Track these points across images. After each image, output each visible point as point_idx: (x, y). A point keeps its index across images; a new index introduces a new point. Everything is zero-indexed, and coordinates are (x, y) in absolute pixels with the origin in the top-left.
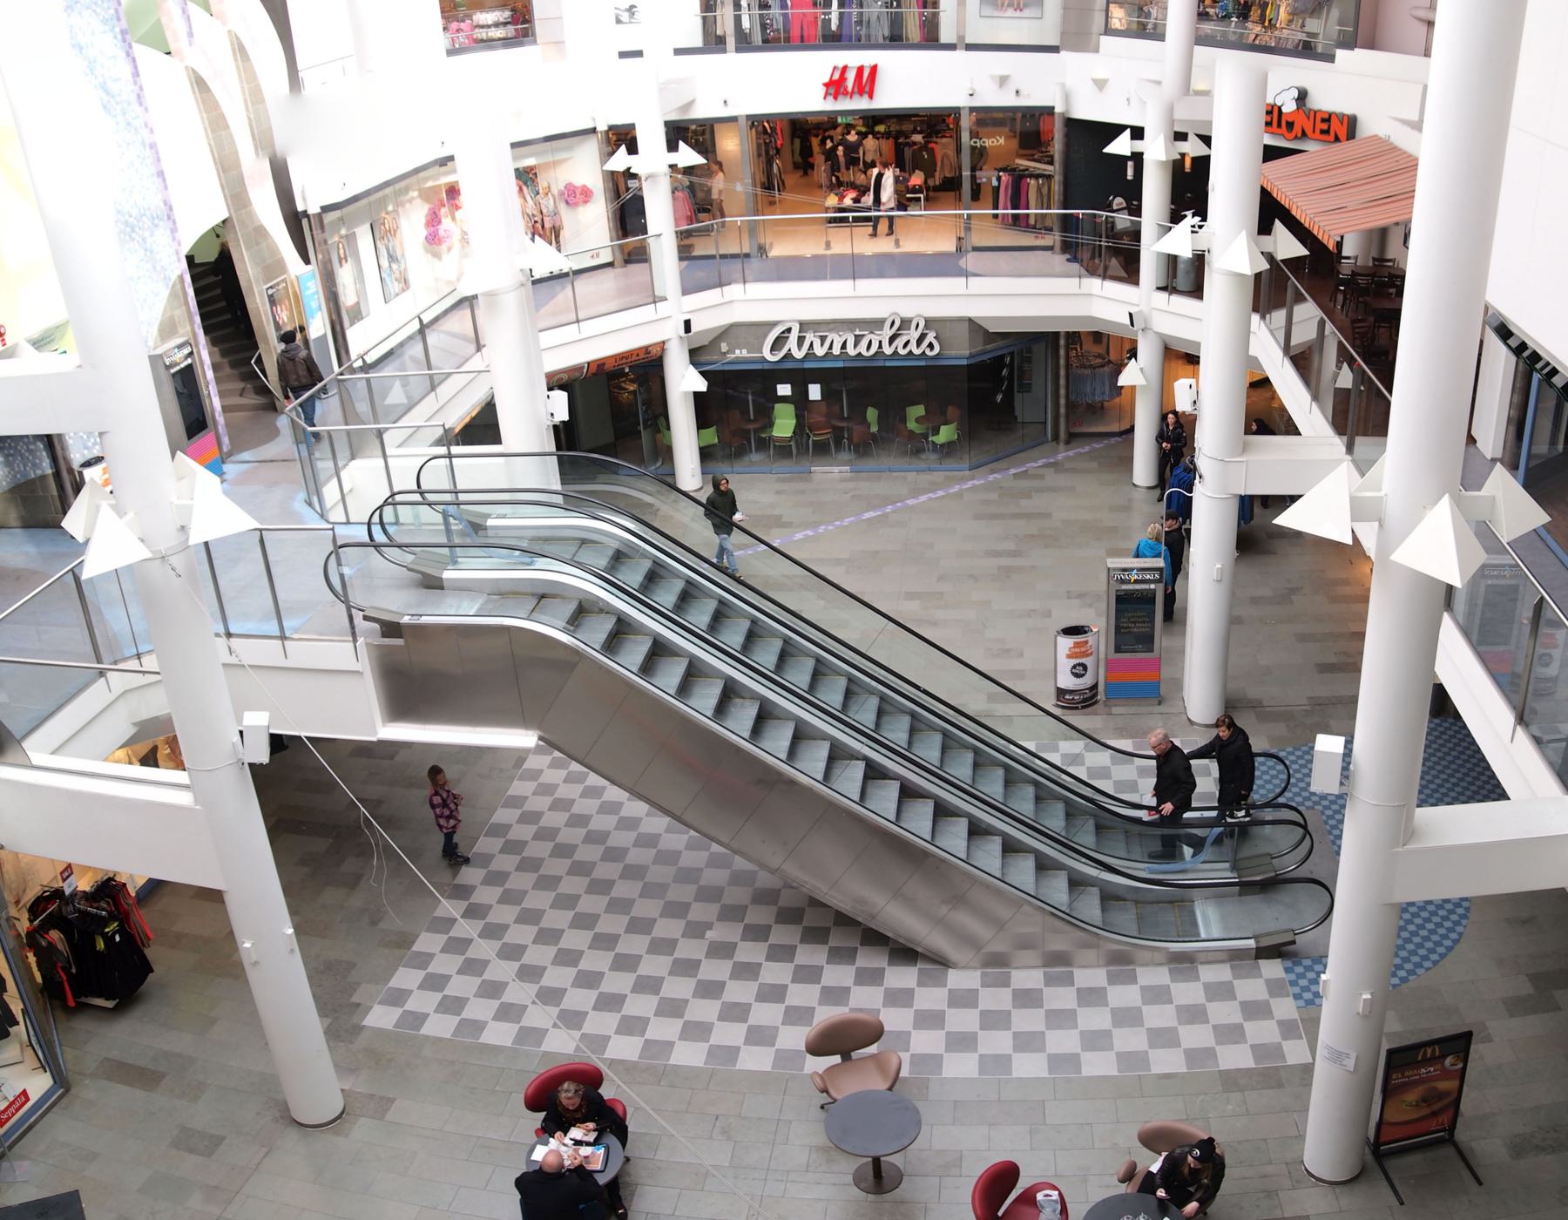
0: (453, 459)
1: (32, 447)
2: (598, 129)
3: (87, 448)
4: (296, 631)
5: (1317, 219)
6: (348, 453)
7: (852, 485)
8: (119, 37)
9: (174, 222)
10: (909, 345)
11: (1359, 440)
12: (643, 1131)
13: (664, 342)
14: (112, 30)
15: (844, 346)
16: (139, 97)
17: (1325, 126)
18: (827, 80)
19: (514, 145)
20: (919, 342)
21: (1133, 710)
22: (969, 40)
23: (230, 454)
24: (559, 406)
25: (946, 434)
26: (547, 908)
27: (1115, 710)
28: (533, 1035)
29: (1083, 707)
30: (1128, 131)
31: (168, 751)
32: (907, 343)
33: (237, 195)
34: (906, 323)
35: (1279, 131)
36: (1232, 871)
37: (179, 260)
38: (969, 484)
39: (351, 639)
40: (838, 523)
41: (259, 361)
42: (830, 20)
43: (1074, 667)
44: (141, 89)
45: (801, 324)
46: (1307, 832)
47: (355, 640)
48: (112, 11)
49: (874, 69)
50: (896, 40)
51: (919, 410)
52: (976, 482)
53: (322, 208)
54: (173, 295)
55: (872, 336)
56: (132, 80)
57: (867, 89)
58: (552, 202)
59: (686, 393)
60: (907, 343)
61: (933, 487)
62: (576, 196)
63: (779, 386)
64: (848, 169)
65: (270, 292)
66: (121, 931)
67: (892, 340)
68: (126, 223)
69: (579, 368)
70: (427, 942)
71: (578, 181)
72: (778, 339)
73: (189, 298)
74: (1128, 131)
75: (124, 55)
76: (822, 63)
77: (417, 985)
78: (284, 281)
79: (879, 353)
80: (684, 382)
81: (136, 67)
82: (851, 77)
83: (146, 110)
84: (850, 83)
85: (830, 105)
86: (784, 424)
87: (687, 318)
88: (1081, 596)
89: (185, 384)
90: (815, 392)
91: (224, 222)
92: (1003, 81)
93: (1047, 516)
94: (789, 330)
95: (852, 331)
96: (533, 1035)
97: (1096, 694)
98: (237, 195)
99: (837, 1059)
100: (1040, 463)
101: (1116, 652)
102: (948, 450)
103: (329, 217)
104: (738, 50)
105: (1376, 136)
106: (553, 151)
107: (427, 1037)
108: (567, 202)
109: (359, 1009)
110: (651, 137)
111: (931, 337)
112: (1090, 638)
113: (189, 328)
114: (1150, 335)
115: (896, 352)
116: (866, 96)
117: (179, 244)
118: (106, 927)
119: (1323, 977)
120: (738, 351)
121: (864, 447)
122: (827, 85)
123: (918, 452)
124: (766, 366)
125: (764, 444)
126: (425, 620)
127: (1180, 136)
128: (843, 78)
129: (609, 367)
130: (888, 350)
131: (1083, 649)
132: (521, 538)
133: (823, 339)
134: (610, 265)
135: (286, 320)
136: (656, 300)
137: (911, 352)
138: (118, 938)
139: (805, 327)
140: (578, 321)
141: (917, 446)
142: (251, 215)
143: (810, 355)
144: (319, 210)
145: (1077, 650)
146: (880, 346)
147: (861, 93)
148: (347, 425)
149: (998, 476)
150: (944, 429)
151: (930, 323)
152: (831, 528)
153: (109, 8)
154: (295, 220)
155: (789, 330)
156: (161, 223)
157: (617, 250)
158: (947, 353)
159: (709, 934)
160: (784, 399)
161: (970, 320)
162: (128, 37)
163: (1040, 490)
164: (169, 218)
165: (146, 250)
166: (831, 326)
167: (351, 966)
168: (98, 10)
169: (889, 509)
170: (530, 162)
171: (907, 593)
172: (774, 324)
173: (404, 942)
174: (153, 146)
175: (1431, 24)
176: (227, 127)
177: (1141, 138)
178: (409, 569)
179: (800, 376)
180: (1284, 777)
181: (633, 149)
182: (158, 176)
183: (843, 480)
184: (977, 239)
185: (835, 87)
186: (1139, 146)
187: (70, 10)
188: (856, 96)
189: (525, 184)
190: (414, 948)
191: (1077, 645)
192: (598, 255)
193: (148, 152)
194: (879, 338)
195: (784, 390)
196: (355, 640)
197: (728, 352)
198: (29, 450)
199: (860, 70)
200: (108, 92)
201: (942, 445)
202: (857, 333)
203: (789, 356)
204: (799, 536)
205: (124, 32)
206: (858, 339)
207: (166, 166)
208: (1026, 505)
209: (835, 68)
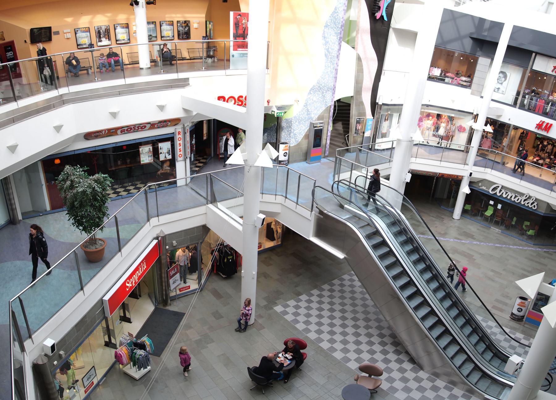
1: (274, 134)
2: (474, 114)
3: (285, 139)
4: (302, 203)
7: (498, 235)
8: (339, 38)
9: (335, 91)
10: (529, 204)
12: (311, 366)
13: (463, 176)
14: (337, 36)
15: (511, 197)
16: (338, 56)
18: (538, 123)
19: (423, 105)
20: (532, 204)
21: (531, 328)
23: (327, 156)
24: (408, 178)
25: (531, 232)
26: (337, 303)
27: (526, 325)
28: (308, 331)
29: (517, 321)
31: (274, 223)
32: (528, 203)
33: (358, 90)
34: (530, 197)
37: (332, 101)
38: (531, 248)
39: (311, 210)
41: (348, 136)
42: (547, 109)
43: (519, 308)
44: (339, 54)
45: (502, 186)
47: (312, 211)
48: (339, 31)
49: (551, 125)
51: (527, 223)
52: (533, 249)
53: (383, 104)
54: (326, 109)
55: (520, 197)
56: (337, 51)
58: (454, 128)
59: (464, 193)
60: (528, 203)
61: (521, 245)
62: (461, 129)
63: (491, 201)
64: (541, 151)
65: (358, 120)
66: (232, 259)
67: (525, 200)
68: (319, 87)
69: (436, 173)
70: (304, 297)
71: (463, 125)
73: (331, 113)
75: (338, 44)
76: (538, 119)
77: (301, 309)
78: (364, 118)
79: (520, 203)
80: (465, 189)
81: (340, 48)
83: (339, 60)
84: (543, 127)
86: (489, 212)
87: (472, 172)
89: (318, 134)
90: (499, 206)
91: (352, 97)
93: (546, 265)
94: (498, 187)
95: (515, 194)
96: (308, 331)
97: (523, 319)
98: (358, 90)
99: (367, 375)
100: (554, 251)
101: (532, 309)
102: (530, 237)
103: (384, 107)
104: (519, 108)
106: (460, 115)
107: (285, 318)
108: (458, 130)
109: (276, 304)
110: (482, 120)
111: (535, 204)
112: (526, 302)
113: (327, 120)
116: (546, 132)
117: (334, 97)
118: (229, 256)
120: (483, 187)
121: (509, 227)
123: (523, 234)
124: (489, 194)
125: (482, 215)
126: (330, 214)
128: (542, 124)
129: (445, 176)
130: (522, 203)
131: (523, 305)
133: (506, 193)
134: (463, 151)
135: (360, 128)
136: (465, 164)
137: (528, 206)
138: (230, 261)
139: (503, 188)
141: (522, 233)
142: (361, 98)
143: (501, 196)
144: (381, 104)
145: (521, 304)
146: (521, 201)
147: (545, 130)
149: (540, 249)
150: (531, 231)
152: (485, 244)
153: (339, 30)
154: (374, 104)
155: (498, 187)
156: (330, 90)
157: (466, 147)
158: (538, 210)
159: (370, 330)
160: (491, 205)
161: (548, 203)
162: (341, 40)
163: (549, 258)
164: (333, 89)
165: (323, 95)
166: (510, 190)
167: (283, 294)
168: (335, 30)
170: (453, 115)
171: (492, 270)
172: (495, 184)
173: (299, 294)
174: (336, 70)
176: (363, 72)
178: (338, 201)
179: (497, 200)
181: (476, 121)
182: (335, 78)
183: (497, 233)
185: (539, 126)
187: (326, 27)
188: (544, 131)
189: (450, 120)
190: (300, 297)
191: (521, 302)
192: (460, 147)
193: (334, 71)
194: (521, 199)
195: (492, 202)
196: (312, 211)
197: (480, 186)
198: (273, 135)
200: (328, 51)
201: (530, 235)
202: (516, 195)
203: (496, 194)
204: (475, 243)
205: (340, 38)
206: (516, 197)
207: (338, 76)
208: (543, 261)
209: (541, 121)
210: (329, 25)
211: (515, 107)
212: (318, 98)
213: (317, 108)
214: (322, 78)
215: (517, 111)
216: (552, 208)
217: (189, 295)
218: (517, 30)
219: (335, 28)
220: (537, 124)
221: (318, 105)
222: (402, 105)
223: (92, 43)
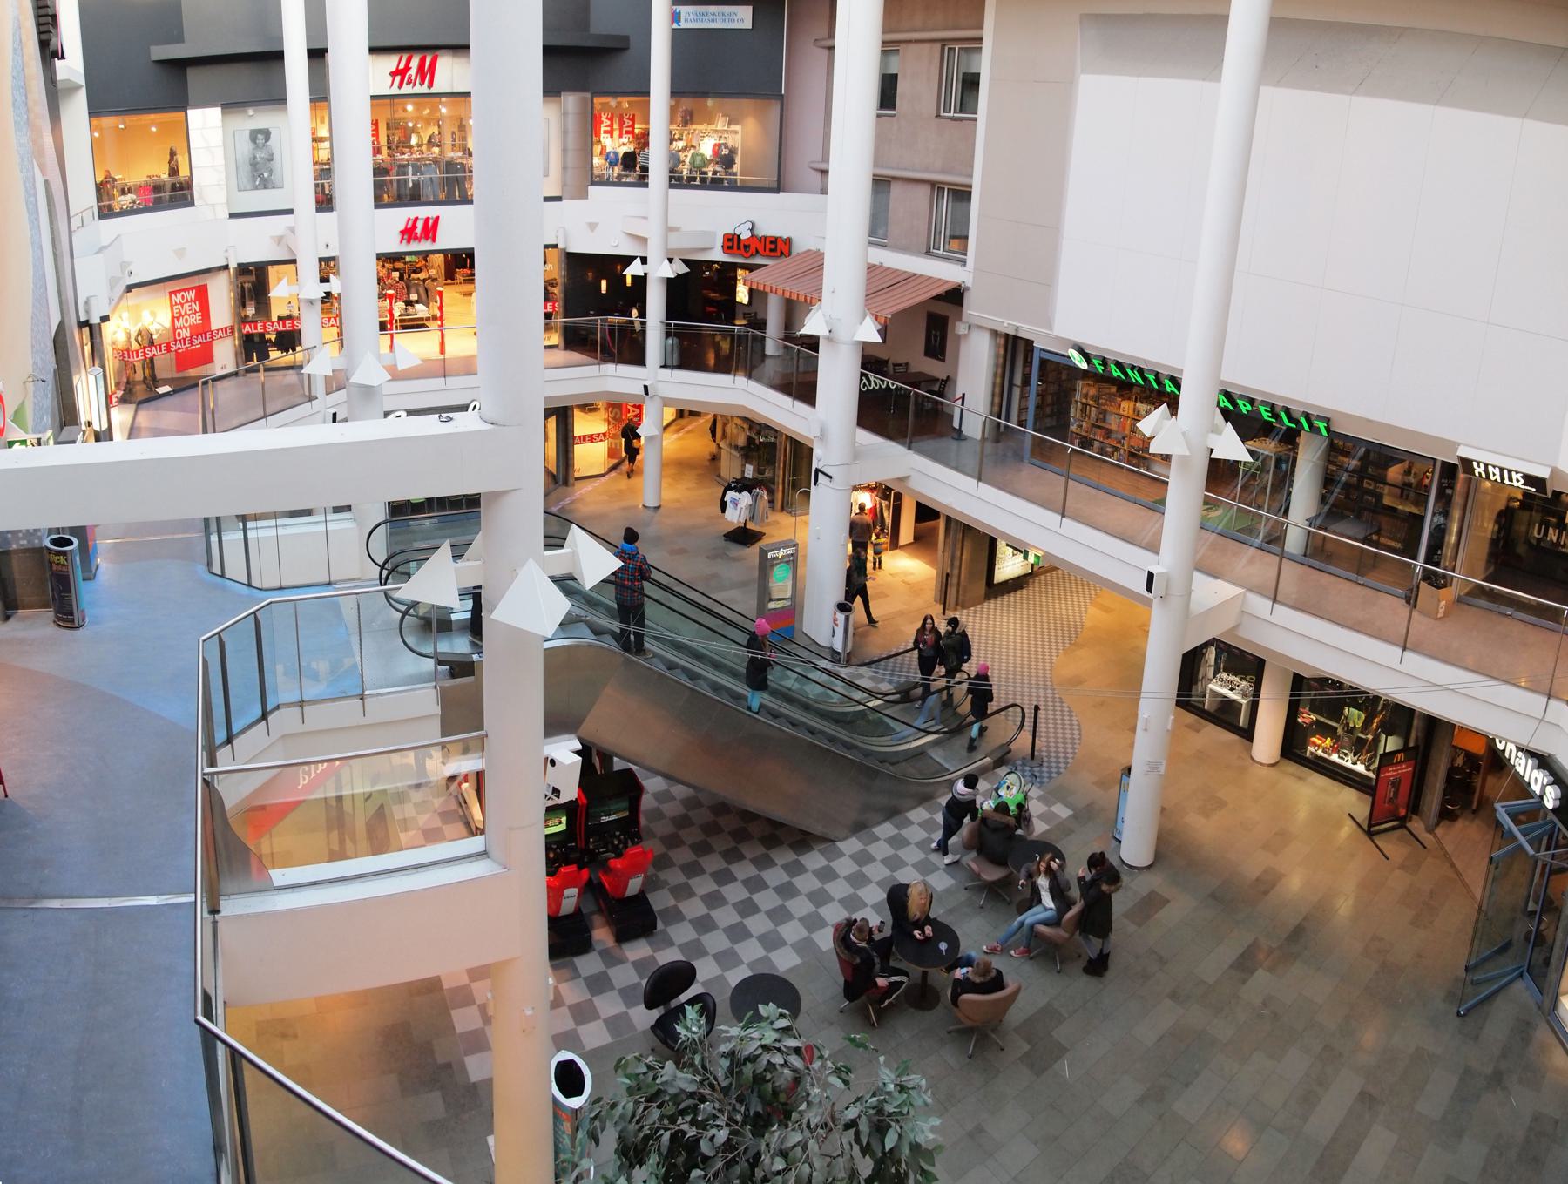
0: (1547, 718)
17: (773, 246)
18: (402, 228)
35: (739, 252)
49: (437, 219)
50: (449, 201)
84: (419, 230)
85: (404, 248)
87: (333, 411)
105: (809, 251)
128: (414, 227)
134: (235, 374)
136: (311, 398)
140: (265, 416)
147: (427, 238)
175: (825, 172)
185: (408, 233)
199: (427, 219)
209: (409, 219)
217: (1555, 1033)
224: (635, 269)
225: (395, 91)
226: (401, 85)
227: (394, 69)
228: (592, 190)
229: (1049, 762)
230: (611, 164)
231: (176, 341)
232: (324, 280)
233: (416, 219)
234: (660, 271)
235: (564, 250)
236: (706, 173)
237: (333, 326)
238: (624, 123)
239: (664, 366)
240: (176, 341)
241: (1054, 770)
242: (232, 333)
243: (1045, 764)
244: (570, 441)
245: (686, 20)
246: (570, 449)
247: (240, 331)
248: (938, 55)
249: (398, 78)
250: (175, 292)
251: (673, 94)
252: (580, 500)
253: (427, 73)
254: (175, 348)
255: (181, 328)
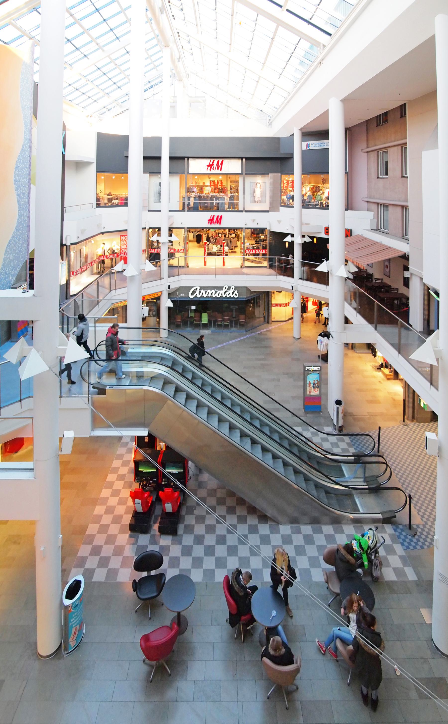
5: (355, 260)
6: (74, 326)
8: (28, 180)
11: (378, 325)
15: (212, 294)
18: (209, 219)
20: (233, 293)
22: (246, 210)
30: (290, 235)
36: (364, 482)
38: (246, 336)
40: (210, 349)
46: (387, 465)
48: (28, 172)
49: (221, 216)
57: (219, 222)
67: (225, 292)
72: (193, 291)
74: (290, 235)
79: (222, 296)
82: (215, 218)
85: (209, 226)
87: (169, 284)
88: (287, 374)
92: (254, 220)
94: (197, 289)
95: (214, 290)
104: (188, 211)
105: (358, 235)
114: (297, 292)
115: (226, 296)
116: (219, 224)
119: (435, 537)
122: (209, 220)
124: (189, 299)
127: (303, 236)
128: (213, 219)
130: (224, 296)
132: (138, 356)
133: (206, 292)
136: (161, 279)
143: (202, 297)
146: (222, 294)
148: (75, 316)
151: (236, 288)
153: (27, 171)
155: (197, 289)
161: (246, 287)
169: (224, 344)
172: (193, 287)
177: (293, 237)
180: (373, 443)
184: (247, 264)
185: (211, 221)
186: (293, 239)
199: (218, 216)
202: (216, 290)
203: (196, 296)
206: (216, 292)
209: (211, 216)
210: (19, 165)
211: (184, 211)
212: (14, 255)
213: (14, 268)
214: (17, 230)
215: (186, 214)
216: (250, 291)
218: (173, 141)
219: (24, 168)
220: (208, 220)
221: (15, 263)
222: (126, 230)
223: (148, 24)
224: (288, 239)
225: (209, 171)
226: (210, 170)
227: (208, 164)
228: (281, 208)
229: (420, 537)
230: (288, 199)
231: (121, 253)
232: (170, 235)
233: (214, 216)
234: (298, 241)
235: (269, 230)
236: (322, 203)
237: (182, 252)
238: (289, 184)
239: (300, 279)
240: (121, 253)
241: (420, 544)
242: (146, 252)
243: (416, 537)
244: (270, 305)
245: (312, 146)
246: (270, 308)
247: (148, 251)
248: (376, 156)
249: (209, 167)
250: (123, 236)
251: (303, 173)
252: (270, 331)
253: (220, 166)
254: (121, 256)
255: (124, 249)
